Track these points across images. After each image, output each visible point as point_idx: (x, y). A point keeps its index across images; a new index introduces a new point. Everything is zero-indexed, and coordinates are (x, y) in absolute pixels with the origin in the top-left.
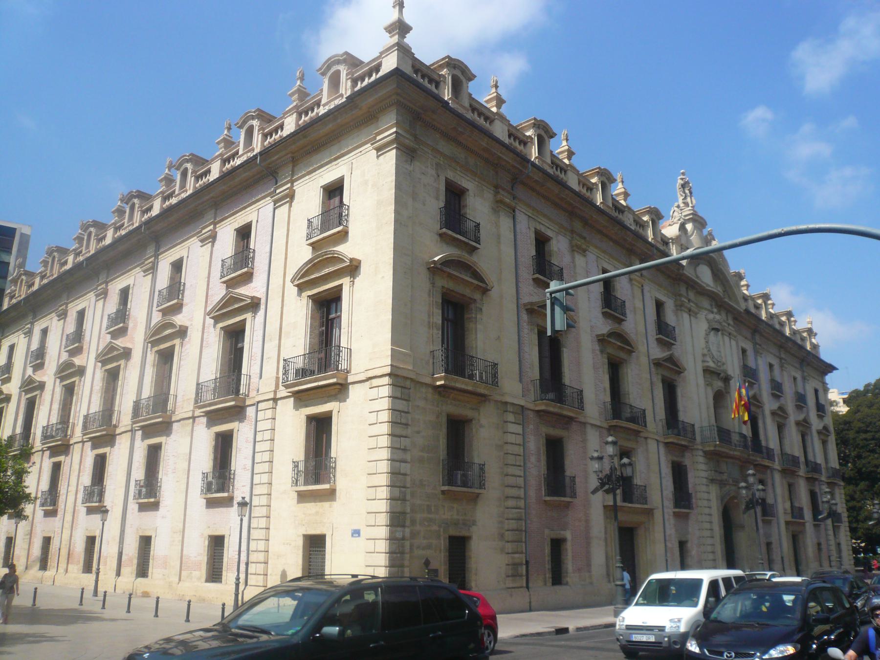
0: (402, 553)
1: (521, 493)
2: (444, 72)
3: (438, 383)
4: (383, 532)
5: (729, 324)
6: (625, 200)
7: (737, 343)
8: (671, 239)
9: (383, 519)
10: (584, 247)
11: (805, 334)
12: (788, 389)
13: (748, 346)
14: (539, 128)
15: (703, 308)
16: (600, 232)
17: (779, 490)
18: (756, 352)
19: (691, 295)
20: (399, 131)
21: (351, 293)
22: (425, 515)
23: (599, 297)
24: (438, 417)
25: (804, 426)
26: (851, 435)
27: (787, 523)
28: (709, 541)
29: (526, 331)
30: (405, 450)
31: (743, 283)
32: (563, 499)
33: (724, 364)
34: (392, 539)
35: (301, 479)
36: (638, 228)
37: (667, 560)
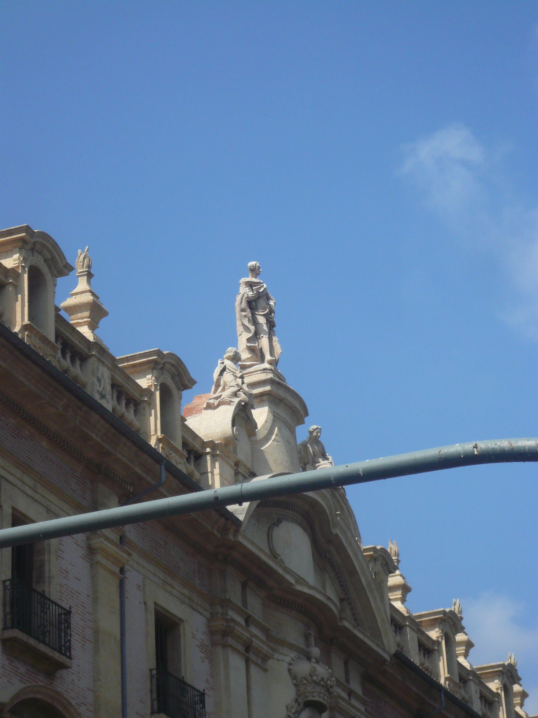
5: (351, 693)
6: (403, 600)
8: (212, 444)
15: (283, 643)
19: (255, 605)
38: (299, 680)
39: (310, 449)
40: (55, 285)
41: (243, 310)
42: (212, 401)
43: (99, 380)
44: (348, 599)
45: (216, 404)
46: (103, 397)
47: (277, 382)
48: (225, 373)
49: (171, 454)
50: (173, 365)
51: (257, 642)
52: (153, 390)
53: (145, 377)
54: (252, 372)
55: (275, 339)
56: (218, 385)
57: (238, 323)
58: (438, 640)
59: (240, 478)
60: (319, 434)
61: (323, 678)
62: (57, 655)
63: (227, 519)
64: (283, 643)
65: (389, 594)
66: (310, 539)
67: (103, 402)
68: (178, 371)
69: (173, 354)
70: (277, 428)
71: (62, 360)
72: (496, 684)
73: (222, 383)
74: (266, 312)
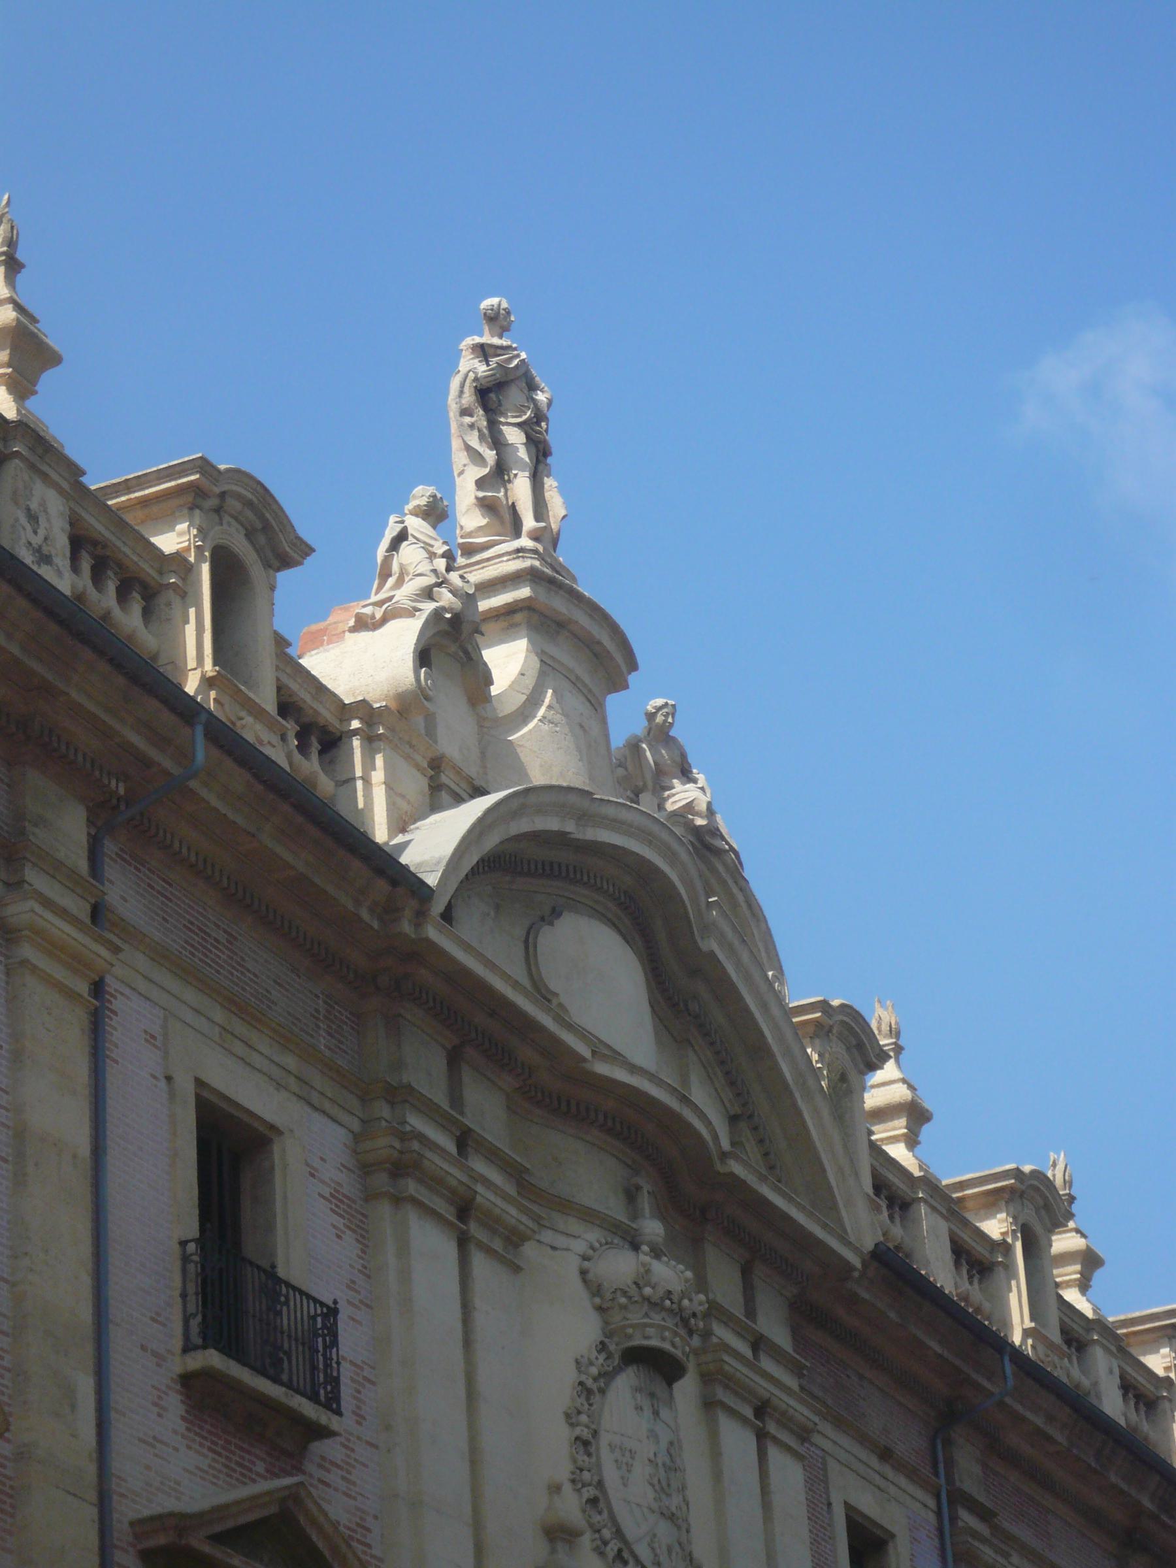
5: (758, 1343)
6: (912, 1141)
7: (817, 1482)
8: (363, 708)
15: (565, 1206)
19: (486, 1107)
31: (884, 1087)
36: (106, 600)
38: (608, 1296)
39: (648, 754)
40: (273, 588)
41: (465, 412)
42: (368, 610)
43: (33, 518)
44: (751, 1117)
45: (378, 615)
46: (46, 559)
47: (549, 579)
48: (405, 543)
49: (241, 719)
50: (249, 504)
51: (438, 1160)
52: (192, 559)
53: (173, 530)
54: (488, 559)
55: (549, 483)
56: (385, 574)
57: (456, 444)
58: (1004, 1241)
59: (445, 796)
60: (670, 720)
61: (670, 1292)
62: (308, 1409)
63: (394, 883)
64: (565, 1206)
65: (1055, 1272)
66: (643, 964)
67: (45, 571)
68: (262, 517)
69: (237, 471)
70: (550, 692)
71: (297, 757)
72: (1164, 1357)
73: (395, 568)
74: (524, 417)
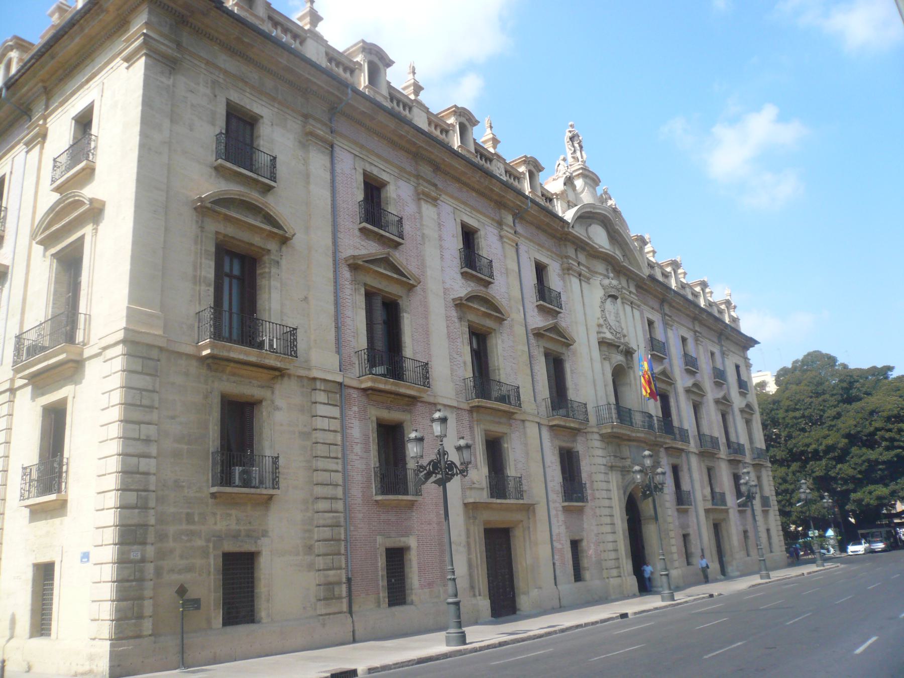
0: (141, 580)
1: (339, 492)
2: (359, 58)
3: (205, 353)
4: (109, 553)
5: (630, 292)
8: (556, 195)
9: (110, 535)
10: (433, 194)
11: (723, 307)
12: (705, 366)
13: (656, 317)
14: (370, 53)
15: (596, 273)
16: (458, 180)
17: (696, 475)
18: (666, 325)
19: (582, 258)
20: (151, 34)
21: (94, 244)
22: (184, 527)
23: (457, 254)
24: (206, 397)
25: (724, 404)
26: (781, 414)
27: (707, 511)
28: (610, 538)
29: (348, 291)
30: (147, 441)
31: (648, 248)
32: (400, 497)
33: (624, 336)
34: (122, 561)
35: (34, 490)
37: (554, 564)
